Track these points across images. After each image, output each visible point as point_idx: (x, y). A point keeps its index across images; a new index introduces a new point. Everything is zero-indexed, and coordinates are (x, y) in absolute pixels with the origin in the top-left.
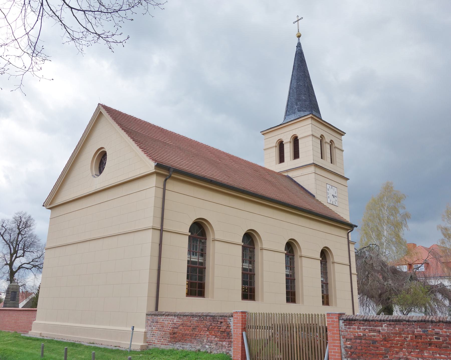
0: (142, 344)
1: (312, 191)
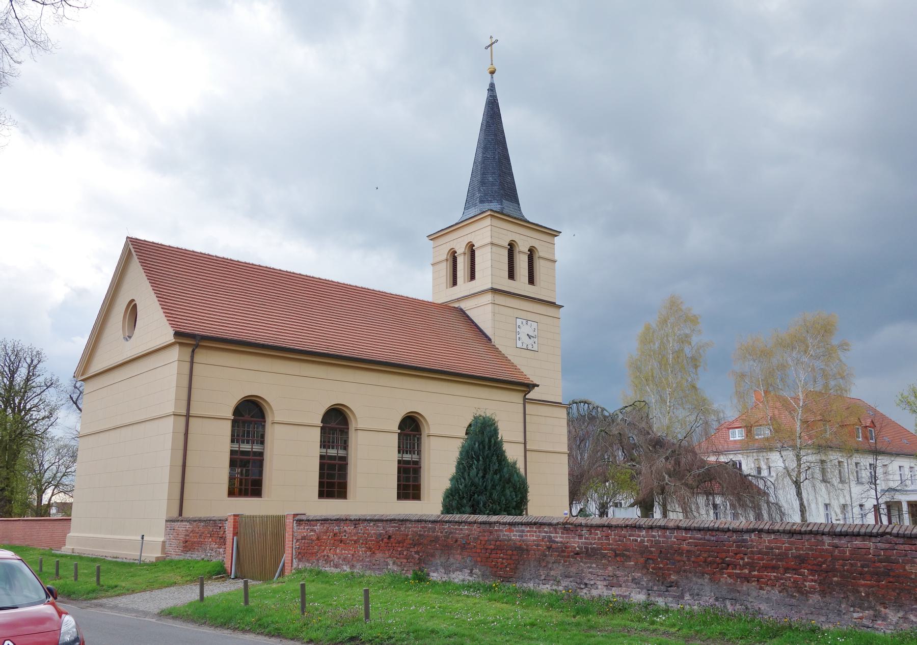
0: (160, 555)
1: (488, 332)
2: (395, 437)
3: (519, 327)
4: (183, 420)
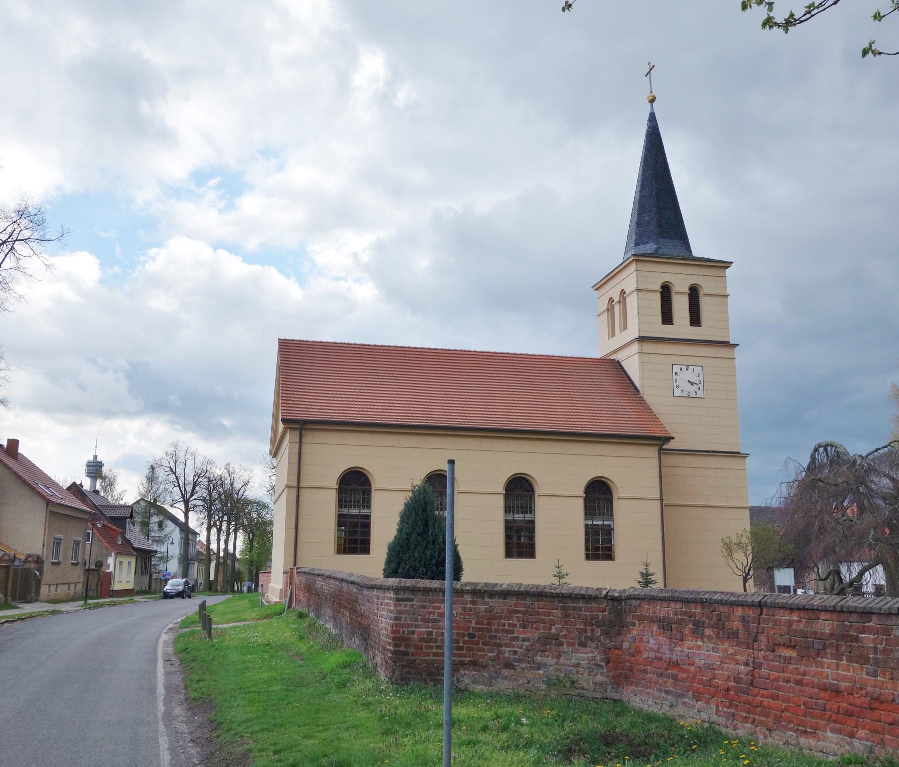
1: (637, 383)
2: (581, 502)
3: (677, 374)
4: (295, 491)
